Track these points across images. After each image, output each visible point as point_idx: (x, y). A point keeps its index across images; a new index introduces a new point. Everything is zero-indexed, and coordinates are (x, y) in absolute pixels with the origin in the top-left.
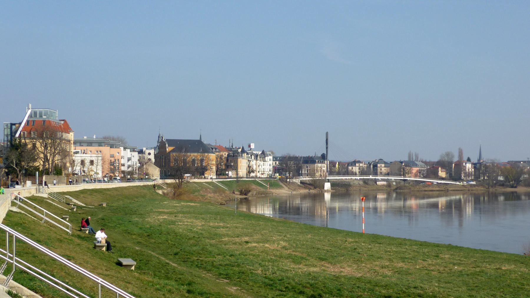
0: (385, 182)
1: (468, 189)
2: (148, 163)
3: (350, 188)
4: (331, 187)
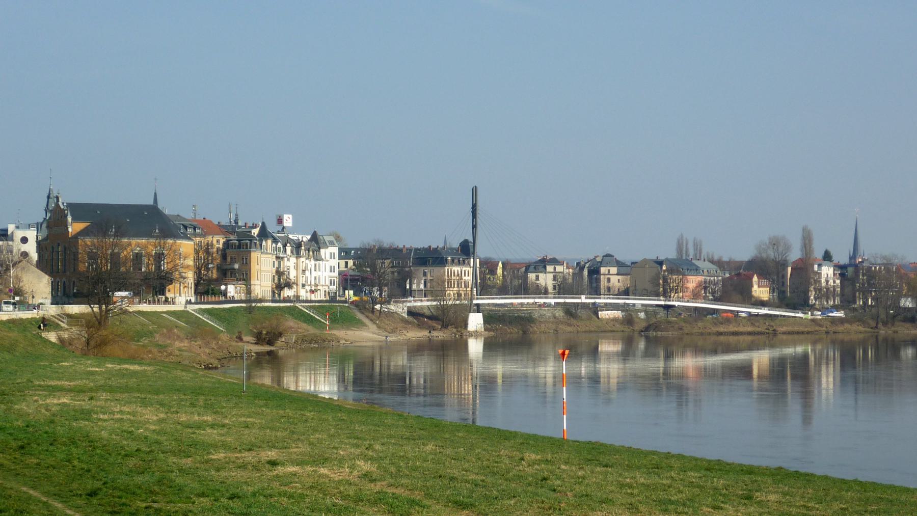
0: (620, 312)
1: (824, 329)
3: (532, 325)
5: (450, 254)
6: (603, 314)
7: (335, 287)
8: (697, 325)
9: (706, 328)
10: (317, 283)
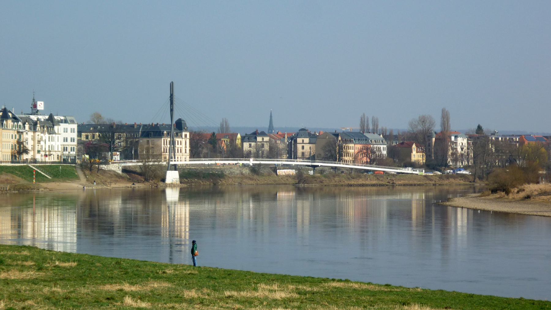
0: (294, 170)
1: (433, 182)
3: (221, 180)
5: (166, 129)
7: (74, 153)
8: (334, 179)
9: (340, 181)
10: (51, 149)
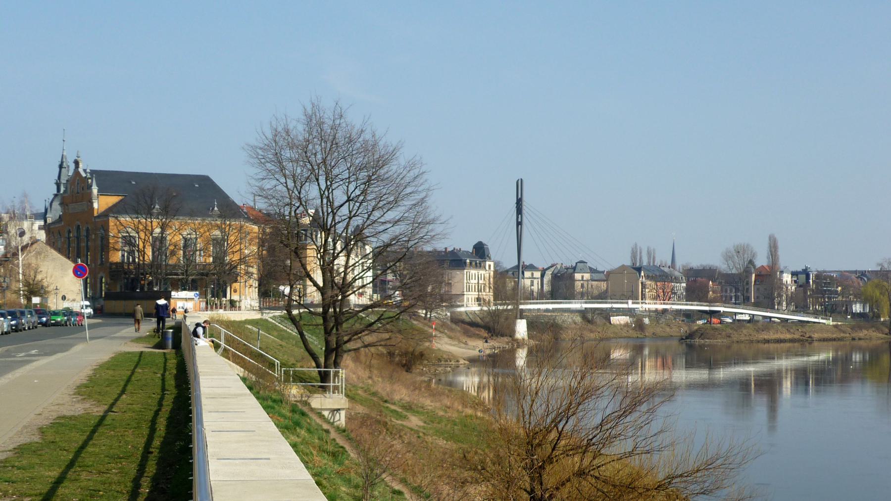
0: (628, 317)
2: (32, 244)
4: (528, 331)
6: (615, 320)
